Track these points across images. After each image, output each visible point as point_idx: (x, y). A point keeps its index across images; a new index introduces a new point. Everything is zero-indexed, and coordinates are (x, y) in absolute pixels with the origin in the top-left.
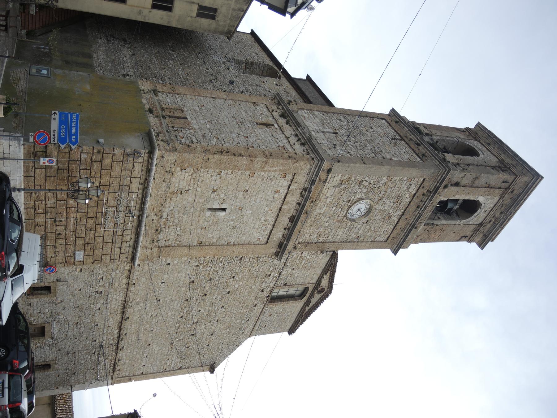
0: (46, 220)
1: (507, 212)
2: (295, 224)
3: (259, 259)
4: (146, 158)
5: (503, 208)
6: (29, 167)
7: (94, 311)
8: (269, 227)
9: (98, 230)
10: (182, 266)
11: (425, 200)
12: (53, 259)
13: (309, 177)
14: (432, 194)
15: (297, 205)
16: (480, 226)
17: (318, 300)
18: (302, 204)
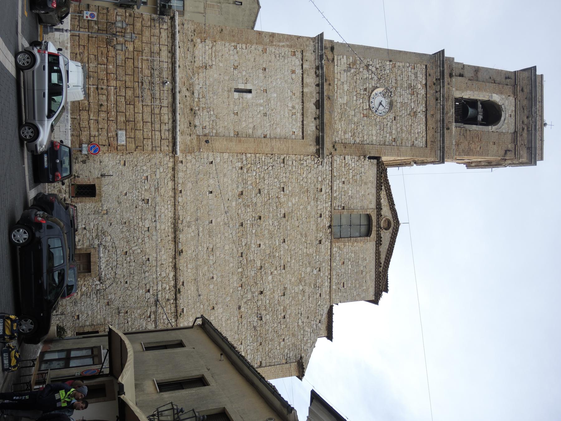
0: (89, 86)
1: (532, 114)
2: (322, 108)
3: (302, 162)
4: (169, 24)
5: (525, 111)
6: (75, 25)
7: (143, 232)
8: (299, 117)
9: (137, 103)
10: (226, 166)
11: (439, 89)
12: (96, 138)
13: (316, 55)
14: (441, 81)
15: (317, 87)
16: (516, 134)
17: (391, 241)
18: (320, 83)
